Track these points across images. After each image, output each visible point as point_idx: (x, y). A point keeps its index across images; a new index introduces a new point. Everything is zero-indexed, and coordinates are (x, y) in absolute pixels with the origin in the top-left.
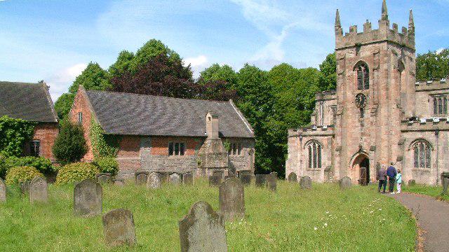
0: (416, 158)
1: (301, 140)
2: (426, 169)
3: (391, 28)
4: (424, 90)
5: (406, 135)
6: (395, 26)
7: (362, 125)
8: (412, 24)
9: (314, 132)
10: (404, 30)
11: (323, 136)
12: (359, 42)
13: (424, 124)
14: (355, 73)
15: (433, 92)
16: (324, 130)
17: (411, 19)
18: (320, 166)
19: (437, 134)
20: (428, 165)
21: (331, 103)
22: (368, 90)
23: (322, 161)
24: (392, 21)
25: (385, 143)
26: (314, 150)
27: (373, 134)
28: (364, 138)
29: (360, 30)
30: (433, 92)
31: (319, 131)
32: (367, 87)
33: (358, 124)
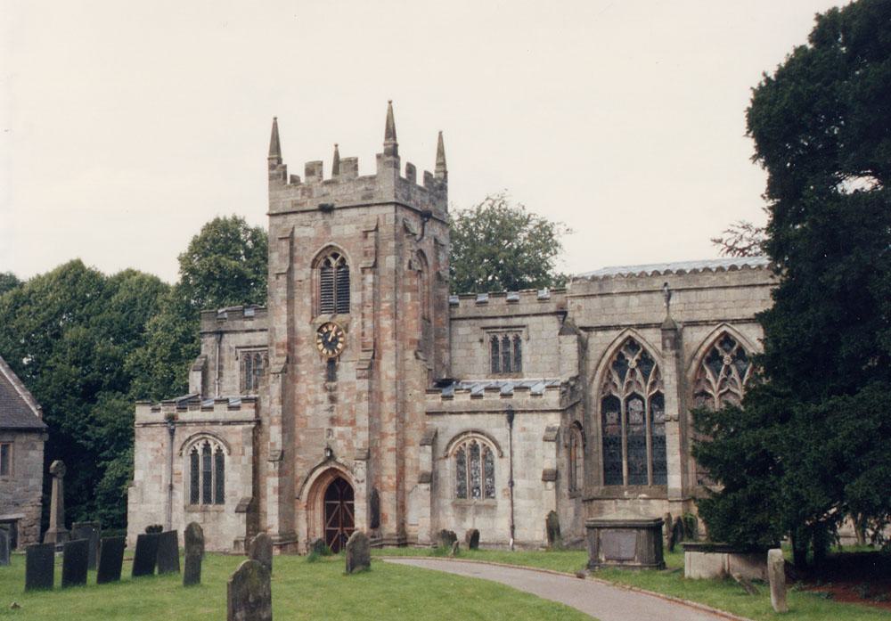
0: (461, 475)
1: (172, 433)
2: (486, 501)
3: (403, 174)
4: (745, 286)
5: (436, 423)
6: (411, 169)
7: (333, 399)
8: (442, 164)
9: (208, 416)
10: (427, 176)
11: (229, 423)
12: (328, 201)
13: (238, 408)
14: (316, 275)
15: (491, 323)
16: (475, 397)
17: (441, 152)
18: (220, 499)
19: (510, 420)
20: (489, 492)
21: (243, 339)
22: (341, 317)
23: (228, 487)
24: (405, 156)
25: (391, 442)
26: (207, 460)
27: (363, 421)
28: (337, 429)
29: (368, 167)
30: (491, 323)
31: (221, 412)
32: (344, 307)
33: (323, 396)
